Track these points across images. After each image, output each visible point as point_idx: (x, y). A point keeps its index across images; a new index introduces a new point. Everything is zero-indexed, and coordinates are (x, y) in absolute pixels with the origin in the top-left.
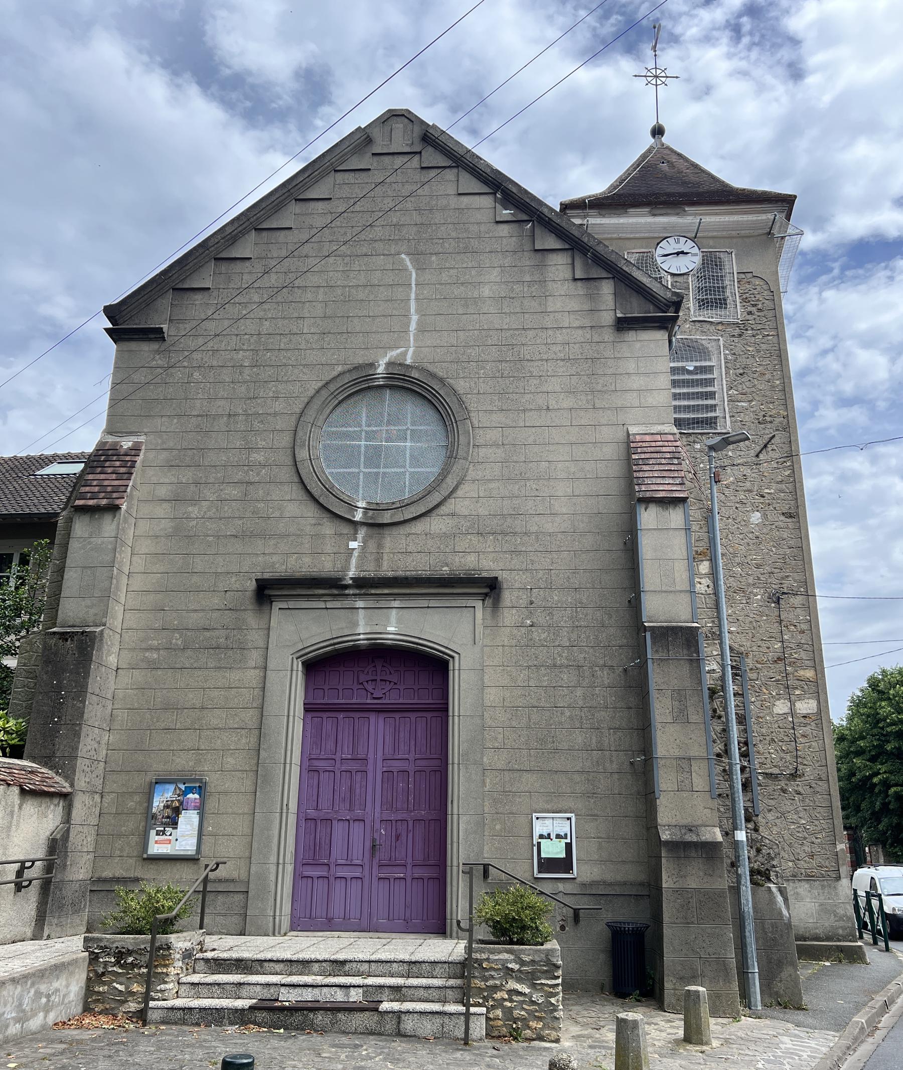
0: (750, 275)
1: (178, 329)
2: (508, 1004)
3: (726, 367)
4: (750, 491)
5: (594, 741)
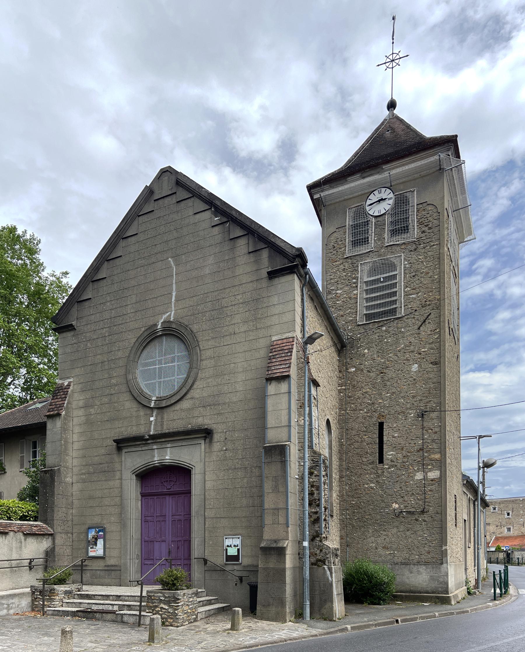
0: (425, 204)
1: (80, 322)
2: (161, 612)
3: (405, 273)
4: (413, 352)
5: (251, 503)
